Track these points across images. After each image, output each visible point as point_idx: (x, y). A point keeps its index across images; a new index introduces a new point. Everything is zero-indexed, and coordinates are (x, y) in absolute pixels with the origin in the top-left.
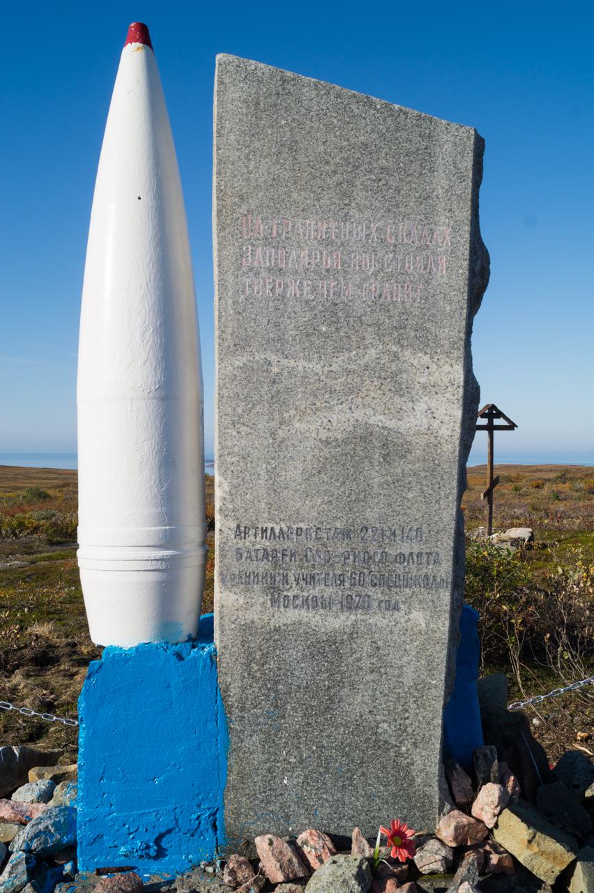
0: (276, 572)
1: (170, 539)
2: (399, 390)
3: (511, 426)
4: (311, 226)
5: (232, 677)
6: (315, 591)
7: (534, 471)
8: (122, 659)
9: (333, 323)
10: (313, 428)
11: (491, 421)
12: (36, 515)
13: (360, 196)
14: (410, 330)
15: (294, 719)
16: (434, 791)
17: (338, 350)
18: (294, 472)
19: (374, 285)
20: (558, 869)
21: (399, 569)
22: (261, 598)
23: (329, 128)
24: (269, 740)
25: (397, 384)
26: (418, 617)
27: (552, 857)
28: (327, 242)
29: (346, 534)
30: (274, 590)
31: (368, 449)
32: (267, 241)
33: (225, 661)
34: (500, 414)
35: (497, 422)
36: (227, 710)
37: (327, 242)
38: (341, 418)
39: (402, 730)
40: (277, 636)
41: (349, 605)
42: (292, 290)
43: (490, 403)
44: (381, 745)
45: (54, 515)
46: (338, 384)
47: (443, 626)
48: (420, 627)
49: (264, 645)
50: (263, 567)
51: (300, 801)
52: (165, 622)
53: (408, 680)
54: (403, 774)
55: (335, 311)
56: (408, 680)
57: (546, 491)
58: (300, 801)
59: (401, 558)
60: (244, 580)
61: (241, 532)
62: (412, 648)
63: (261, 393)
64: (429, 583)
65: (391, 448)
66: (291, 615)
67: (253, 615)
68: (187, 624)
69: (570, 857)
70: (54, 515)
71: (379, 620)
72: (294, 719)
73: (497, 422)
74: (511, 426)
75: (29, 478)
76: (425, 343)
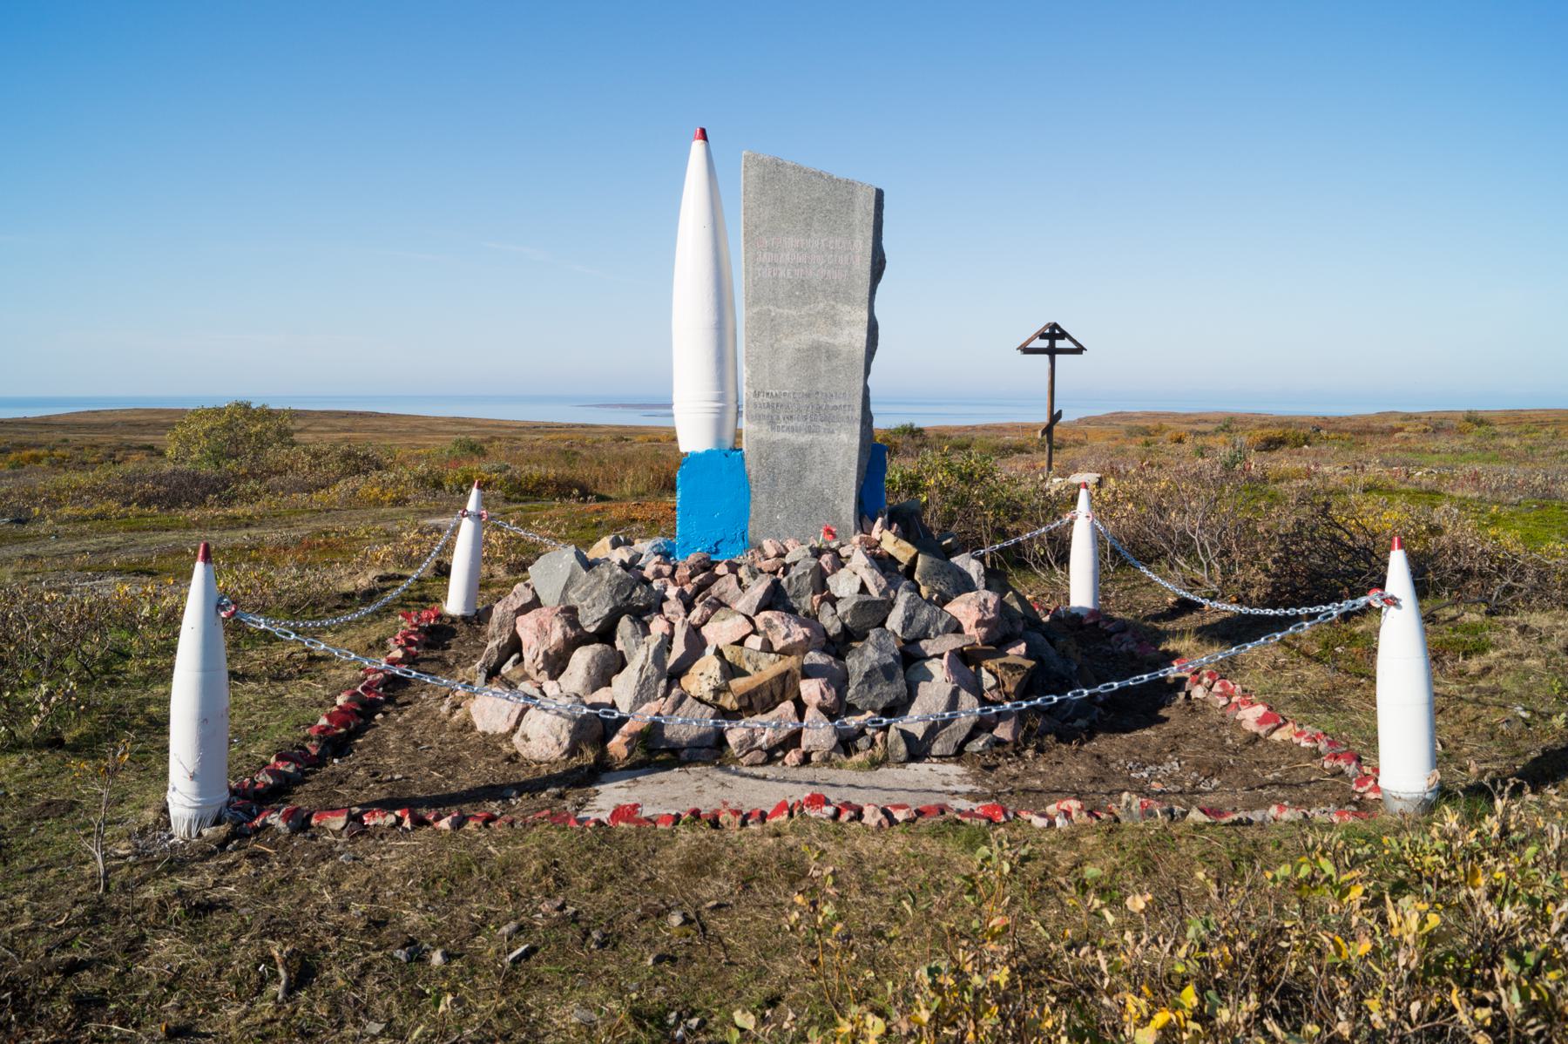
0: (773, 413)
1: (721, 398)
2: (835, 324)
3: (1026, 350)
4: (791, 242)
5: (752, 466)
6: (792, 424)
7: (1195, 423)
8: (696, 457)
9: (802, 290)
10: (792, 343)
11: (1052, 344)
12: (486, 467)
13: (816, 225)
14: (840, 294)
15: (782, 487)
16: (852, 523)
17: (805, 304)
18: (782, 365)
19: (823, 271)
20: (909, 556)
21: (834, 412)
22: (766, 427)
23: (800, 190)
24: (770, 497)
25: (834, 321)
26: (844, 437)
27: (906, 550)
28: (799, 249)
29: (808, 395)
30: (772, 423)
31: (819, 353)
32: (769, 249)
33: (748, 458)
34: (1064, 335)
35: (1059, 344)
36: (749, 481)
37: (799, 249)
38: (805, 338)
39: (836, 492)
40: (774, 446)
41: (809, 431)
42: (782, 274)
43: (1052, 321)
44: (825, 500)
45: (508, 467)
46: (804, 322)
47: (856, 441)
48: (844, 444)
49: (768, 450)
50: (767, 412)
51: (785, 526)
52: (719, 440)
53: (838, 468)
54: (836, 515)
55: (803, 284)
56: (838, 468)
57: (1187, 447)
58: (785, 526)
59: (835, 407)
60: (756, 418)
61: (756, 394)
62: (841, 452)
63: (765, 326)
64: (850, 420)
65: (831, 353)
66: (779, 436)
67: (762, 435)
68: (729, 443)
69: (914, 551)
70: (508, 467)
71: (824, 438)
72: (782, 487)
73: (1059, 344)
74: (1079, 350)
75: (432, 432)
76: (849, 300)
